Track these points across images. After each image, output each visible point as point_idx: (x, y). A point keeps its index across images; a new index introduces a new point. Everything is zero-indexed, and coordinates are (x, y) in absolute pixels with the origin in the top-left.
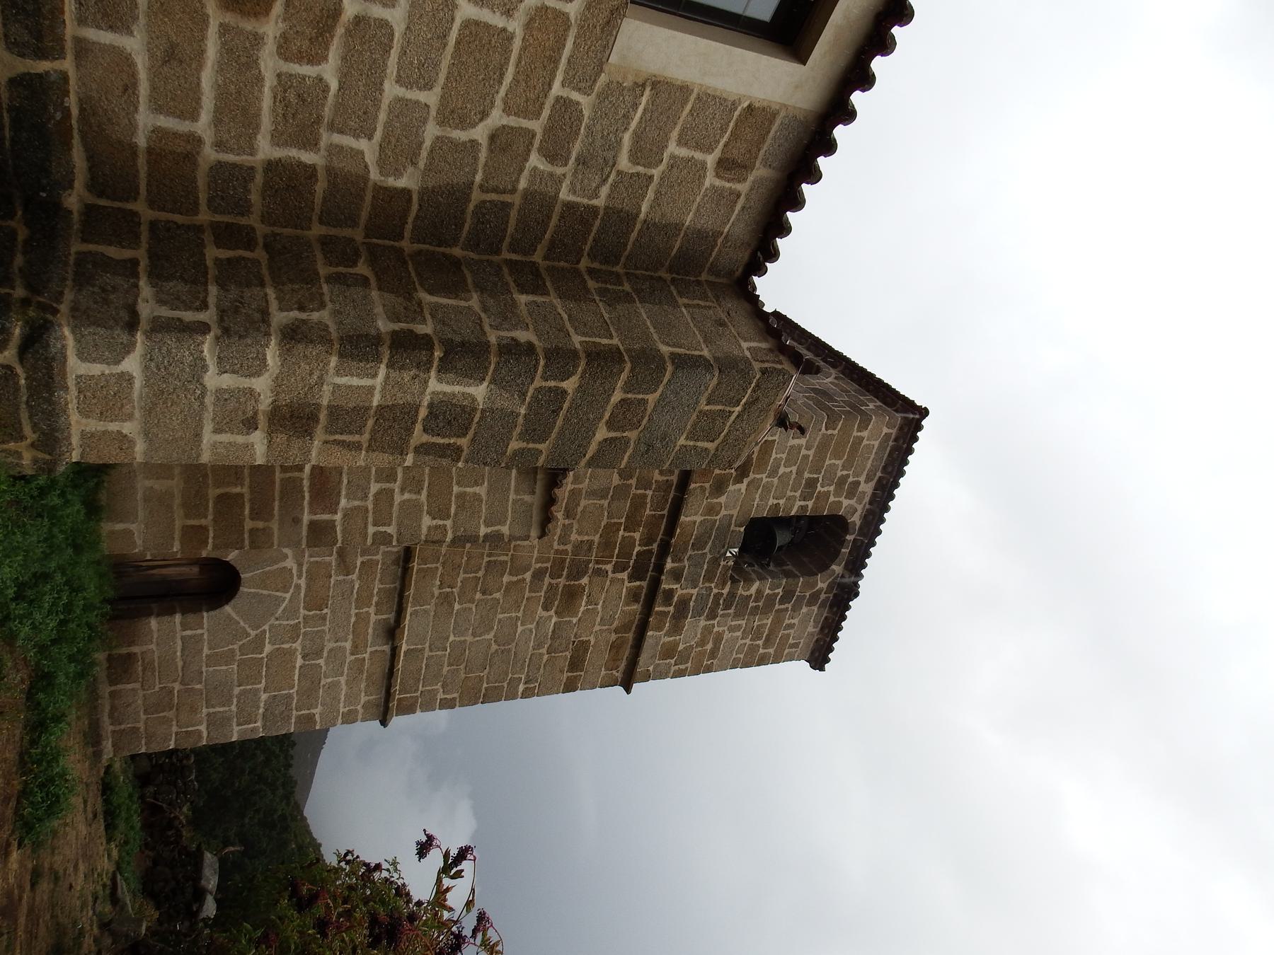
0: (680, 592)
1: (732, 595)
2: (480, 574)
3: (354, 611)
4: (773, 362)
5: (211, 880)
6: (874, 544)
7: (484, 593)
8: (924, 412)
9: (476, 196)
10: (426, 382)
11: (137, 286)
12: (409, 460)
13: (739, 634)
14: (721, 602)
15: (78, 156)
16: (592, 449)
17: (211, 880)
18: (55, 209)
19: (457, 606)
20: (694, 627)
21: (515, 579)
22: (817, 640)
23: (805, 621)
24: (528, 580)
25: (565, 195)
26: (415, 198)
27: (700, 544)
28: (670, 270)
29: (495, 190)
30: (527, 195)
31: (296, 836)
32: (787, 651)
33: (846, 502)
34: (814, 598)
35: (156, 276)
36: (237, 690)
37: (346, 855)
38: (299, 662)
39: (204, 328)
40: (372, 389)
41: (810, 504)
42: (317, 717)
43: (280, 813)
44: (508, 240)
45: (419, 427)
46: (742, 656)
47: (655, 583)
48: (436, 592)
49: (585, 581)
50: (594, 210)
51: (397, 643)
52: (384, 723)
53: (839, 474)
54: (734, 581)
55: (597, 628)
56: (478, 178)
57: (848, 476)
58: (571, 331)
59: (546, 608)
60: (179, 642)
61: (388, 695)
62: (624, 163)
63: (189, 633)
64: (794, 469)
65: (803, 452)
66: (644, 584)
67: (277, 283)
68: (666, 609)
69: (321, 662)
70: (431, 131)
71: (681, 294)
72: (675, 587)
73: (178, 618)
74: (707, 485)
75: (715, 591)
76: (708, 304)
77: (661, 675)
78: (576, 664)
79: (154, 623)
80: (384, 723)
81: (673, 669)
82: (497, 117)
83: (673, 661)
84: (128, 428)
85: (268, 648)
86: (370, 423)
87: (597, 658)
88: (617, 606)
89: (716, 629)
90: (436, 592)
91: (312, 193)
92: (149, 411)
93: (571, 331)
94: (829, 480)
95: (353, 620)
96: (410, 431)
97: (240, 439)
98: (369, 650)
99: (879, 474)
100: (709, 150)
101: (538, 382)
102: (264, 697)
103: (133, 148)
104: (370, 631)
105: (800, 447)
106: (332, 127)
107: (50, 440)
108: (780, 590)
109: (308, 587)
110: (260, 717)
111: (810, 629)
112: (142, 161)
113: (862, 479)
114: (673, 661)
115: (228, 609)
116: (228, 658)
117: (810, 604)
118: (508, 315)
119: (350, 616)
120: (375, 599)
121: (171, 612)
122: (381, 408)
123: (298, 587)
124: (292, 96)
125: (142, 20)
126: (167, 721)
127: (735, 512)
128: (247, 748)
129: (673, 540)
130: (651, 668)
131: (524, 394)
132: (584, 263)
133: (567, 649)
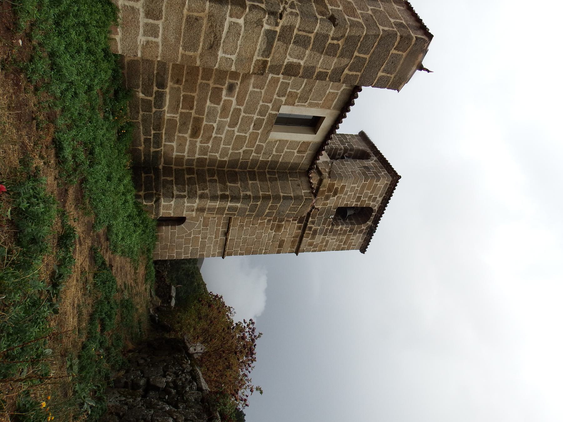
0: (314, 227)
1: (332, 229)
2: (252, 220)
3: (215, 228)
4: (309, 196)
5: (174, 294)
6: (381, 217)
7: (253, 225)
8: (400, 177)
9: (241, 161)
10: (227, 204)
11: (173, 187)
12: (224, 216)
13: (335, 241)
14: (328, 231)
15: (162, 160)
16: (266, 213)
17: (174, 294)
18: (158, 169)
19: (245, 228)
20: (318, 239)
21: (262, 221)
22: (362, 244)
23: (358, 239)
24: (266, 222)
25: (261, 159)
26: (227, 162)
27: (321, 214)
28: (289, 170)
29: (245, 159)
30: (252, 160)
31: (197, 280)
32: (351, 247)
33: (372, 203)
34: (361, 232)
35: (177, 184)
36: (184, 246)
37: (210, 293)
38: (200, 240)
39: (185, 196)
40: (216, 205)
41: (359, 203)
42: (205, 254)
43: (191, 272)
44: (248, 167)
45: (226, 211)
46: (336, 247)
47: (306, 225)
48: (239, 224)
49: (283, 223)
50: (268, 161)
51: (227, 237)
52: (223, 258)
53: (369, 195)
54: (333, 225)
55: (287, 236)
56: (241, 158)
57: (373, 195)
58: (260, 191)
59: (271, 230)
60: (170, 233)
61: (224, 251)
62: (274, 153)
63: (172, 231)
64: (353, 193)
65: (356, 188)
66: (302, 225)
67: (199, 184)
68: (310, 232)
69: (206, 240)
70: (230, 151)
71: (290, 177)
72: (312, 226)
73: (170, 227)
74: (323, 197)
75: (326, 228)
76: (297, 179)
77: (308, 251)
78: (280, 246)
79: (164, 228)
80: (223, 258)
81: (312, 249)
82: (244, 148)
83: (312, 247)
84: (170, 212)
85: (192, 236)
86: (216, 210)
87: (287, 245)
88: (294, 230)
89: (327, 239)
90: (239, 224)
91: (206, 162)
92: (174, 209)
93: (260, 191)
94: (366, 196)
95: (215, 230)
96: (224, 211)
97: (191, 213)
98: (219, 238)
99: (384, 195)
100: (295, 149)
101: (251, 203)
102: (191, 248)
103: (172, 158)
104: (220, 233)
105: (355, 187)
106: (210, 152)
107: (157, 214)
108: (349, 228)
109: (203, 221)
110: (190, 253)
111: (360, 240)
112: (174, 160)
113: (378, 196)
114: (312, 247)
115: (182, 225)
116: (182, 237)
117: (359, 233)
118: (246, 188)
119: (214, 229)
120: (222, 225)
121: (168, 225)
122: (218, 208)
123: (201, 221)
124: (202, 149)
125: (176, 141)
126: (166, 252)
127: (333, 205)
128: (188, 261)
129: (312, 213)
130: (305, 249)
131: (249, 205)
132: (267, 170)
133: (278, 241)
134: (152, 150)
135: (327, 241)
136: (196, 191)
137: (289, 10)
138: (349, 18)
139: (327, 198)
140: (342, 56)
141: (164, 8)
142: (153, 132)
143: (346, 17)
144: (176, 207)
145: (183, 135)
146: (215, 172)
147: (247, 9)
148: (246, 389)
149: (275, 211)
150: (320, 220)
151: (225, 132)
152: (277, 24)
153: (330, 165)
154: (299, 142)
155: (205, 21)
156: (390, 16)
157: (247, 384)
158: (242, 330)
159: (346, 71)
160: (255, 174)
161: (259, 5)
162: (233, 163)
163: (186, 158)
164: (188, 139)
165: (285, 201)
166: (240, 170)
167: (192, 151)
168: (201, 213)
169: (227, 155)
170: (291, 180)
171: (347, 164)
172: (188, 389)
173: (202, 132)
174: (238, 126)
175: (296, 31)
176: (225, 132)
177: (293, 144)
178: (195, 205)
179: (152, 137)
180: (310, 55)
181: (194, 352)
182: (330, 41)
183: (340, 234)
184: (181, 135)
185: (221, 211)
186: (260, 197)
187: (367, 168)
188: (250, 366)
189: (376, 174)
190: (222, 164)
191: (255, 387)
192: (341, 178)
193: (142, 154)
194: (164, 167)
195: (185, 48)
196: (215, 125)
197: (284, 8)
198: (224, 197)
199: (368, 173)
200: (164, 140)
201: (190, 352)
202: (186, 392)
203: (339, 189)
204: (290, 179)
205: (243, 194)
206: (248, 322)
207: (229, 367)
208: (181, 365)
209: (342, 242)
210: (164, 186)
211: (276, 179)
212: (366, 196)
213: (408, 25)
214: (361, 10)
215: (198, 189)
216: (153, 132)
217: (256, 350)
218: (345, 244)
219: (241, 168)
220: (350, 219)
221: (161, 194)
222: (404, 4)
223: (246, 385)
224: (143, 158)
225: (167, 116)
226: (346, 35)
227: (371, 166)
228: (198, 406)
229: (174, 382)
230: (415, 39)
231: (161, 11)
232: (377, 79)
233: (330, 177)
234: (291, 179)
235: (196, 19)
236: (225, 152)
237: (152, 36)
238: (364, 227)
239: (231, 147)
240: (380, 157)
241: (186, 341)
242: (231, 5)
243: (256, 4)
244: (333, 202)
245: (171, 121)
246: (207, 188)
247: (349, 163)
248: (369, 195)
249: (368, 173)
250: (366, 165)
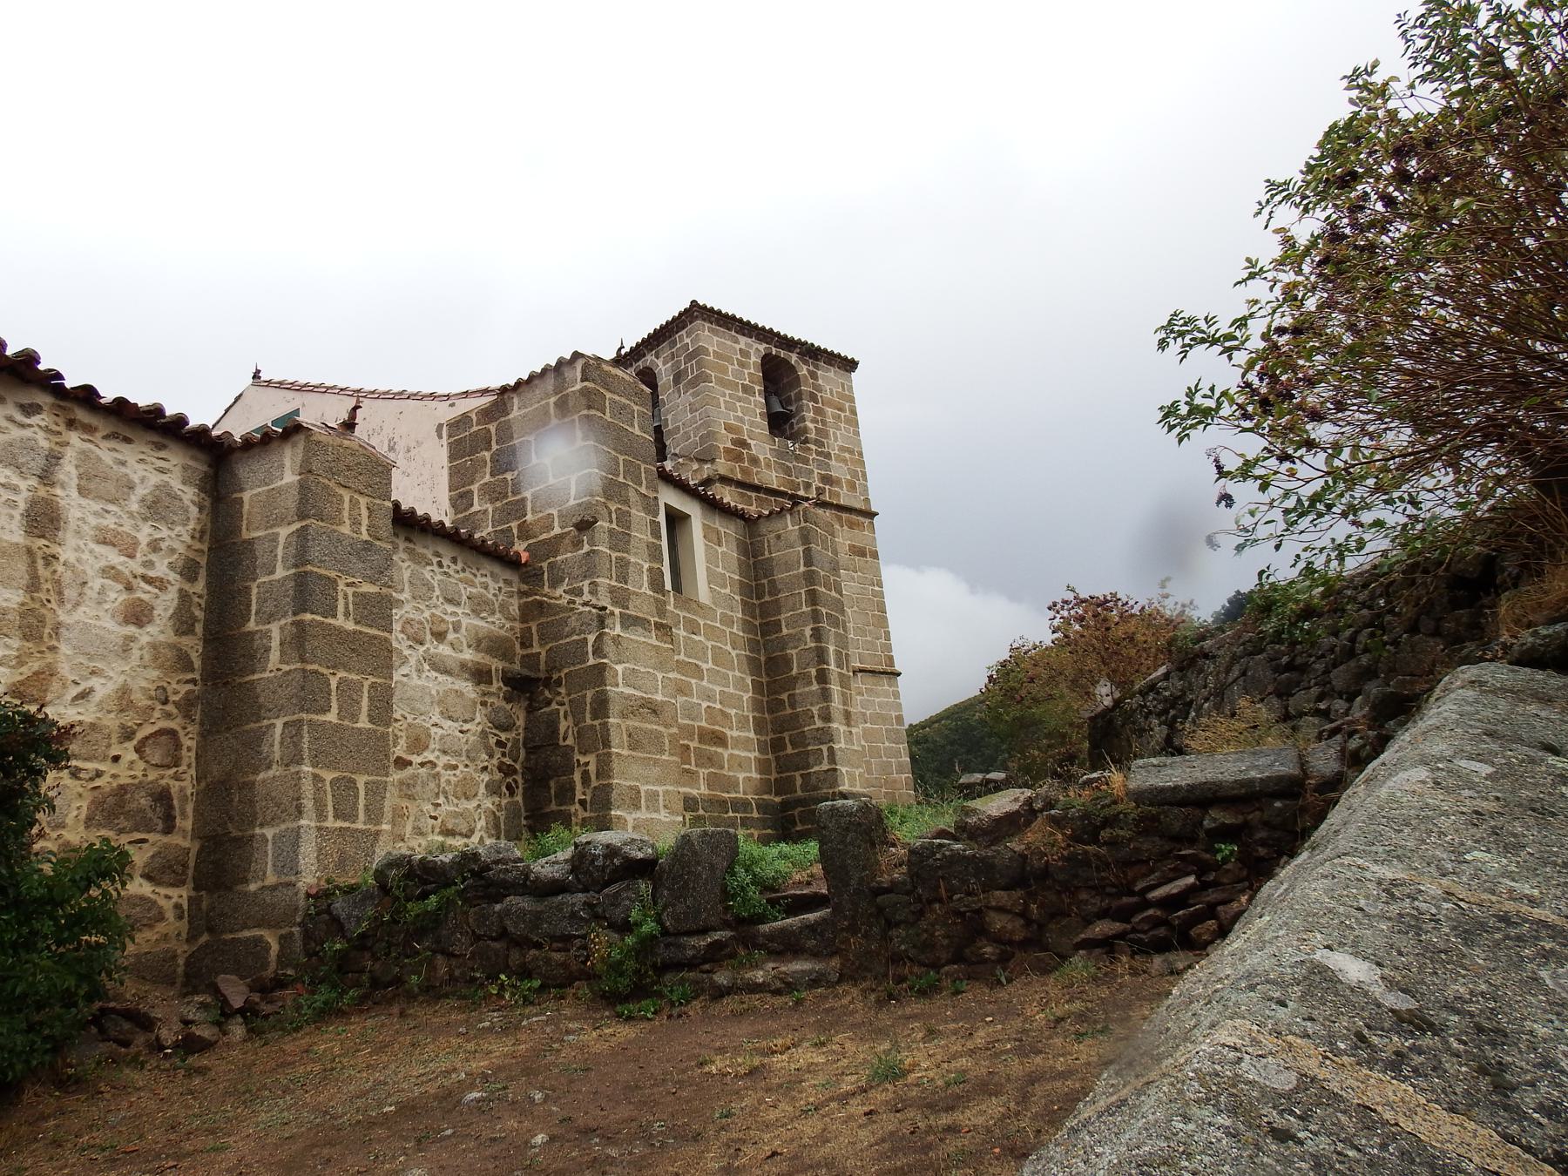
1: (817, 442)
8: (694, 304)
15: (765, 797)
16: (838, 596)
18: (783, 803)
20: (838, 470)
23: (828, 377)
33: (753, 359)
34: (813, 375)
35: (808, 766)
38: (868, 725)
41: (757, 388)
52: (899, 674)
54: (806, 441)
64: (738, 404)
65: (727, 399)
67: (802, 726)
70: (737, 674)
71: (763, 554)
78: (861, 552)
80: (899, 674)
82: (729, 648)
94: (740, 375)
105: (725, 402)
113: (738, 347)
117: (816, 379)
118: (798, 638)
126: (900, 795)
127: (768, 447)
134: (755, 815)
135: (842, 449)
136: (818, 729)
137: (586, 597)
139: (754, 461)
140: (626, 502)
141: (628, 784)
142: (731, 814)
144: (849, 763)
150: (800, 472)
152: (612, 614)
155: (629, 723)
157: (1156, 604)
160: (767, 624)
162: (754, 666)
163: (757, 754)
164: (730, 751)
165: (815, 562)
167: (743, 743)
169: (743, 679)
170: (770, 553)
171: (675, 420)
172: (1167, 694)
173: (717, 728)
174: (700, 663)
175: (614, 583)
177: (711, 558)
178: (843, 728)
179: (738, 815)
180: (636, 554)
181: (1110, 698)
183: (824, 423)
187: (678, 378)
189: (690, 357)
190: (757, 687)
191: (1160, 591)
192: (711, 435)
195: (662, 752)
196: (705, 705)
197: (585, 604)
198: (822, 677)
199: (692, 373)
204: (767, 554)
206: (1052, 613)
207: (1131, 638)
208: (1135, 711)
209: (839, 416)
210: (816, 788)
211: (772, 583)
212: (740, 375)
216: (731, 814)
220: (789, 401)
224: (769, 831)
228: (1189, 674)
229: (1159, 715)
230: (586, 383)
231: (631, 788)
233: (713, 461)
235: (630, 736)
236: (740, 683)
238: (803, 371)
239: (730, 673)
243: (590, 649)
244: (762, 446)
245: (712, 781)
247: (669, 417)
249: (692, 373)
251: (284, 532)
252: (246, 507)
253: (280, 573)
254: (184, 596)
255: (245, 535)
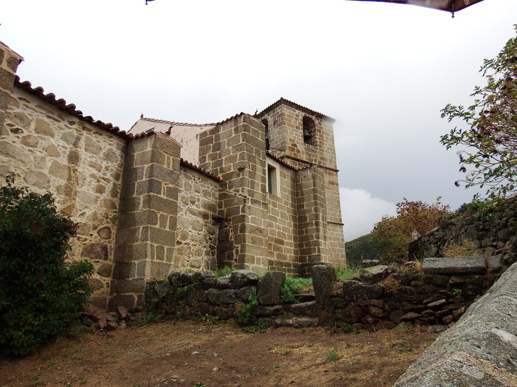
1: (320, 146)
9: (292, 214)
15: (296, 262)
20: (326, 155)
25: (291, 202)
33: (300, 117)
34: (320, 124)
35: (311, 253)
36: (337, 253)
38: (332, 241)
41: (301, 127)
52: (343, 225)
54: (316, 145)
62: (287, 194)
64: (294, 132)
65: (291, 130)
70: (289, 221)
74: (298, 154)
75: (319, 150)
77: (335, 162)
78: (333, 183)
82: (286, 212)
87: (332, 178)
89: (326, 149)
92: (326, 254)
96: (324, 224)
99: (294, 109)
102: (338, 248)
105: (290, 131)
112: (296, 256)
113: (295, 113)
118: (310, 211)
126: (342, 265)
127: (303, 147)
134: (292, 268)
135: (328, 148)
136: (315, 241)
137: (240, 193)
138: (238, 160)
139: (298, 151)
140: (255, 162)
141: (251, 255)
143: (237, 162)
145: (283, 249)
146: (300, 230)
147: (245, 214)
148: (438, 207)
149: (322, 191)
151: (280, 225)
152: (248, 199)
153: (274, 150)
154: (281, 178)
155: (252, 235)
156: (230, 136)
157: (435, 206)
158: (403, 210)
159: (261, 159)
160: (300, 205)
161: (241, 208)
162: (294, 219)
163: (294, 248)
166: (297, 214)
168: (327, 238)
169: (291, 223)
173: (281, 238)
174: (276, 217)
176: (280, 225)
177: (282, 182)
178: (323, 241)
179: (287, 268)
180: (257, 179)
181: (417, 237)
182: (251, 170)
183: (322, 140)
184: (283, 251)
185: (324, 226)
186: (315, 202)
187: (275, 123)
188: (425, 205)
189: (279, 116)
190: (295, 226)
192: (284, 142)
193: (295, 274)
194: (300, 262)
195: (262, 245)
196: (277, 231)
198: (317, 224)
199: (280, 121)
200: (287, 261)
201: (417, 239)
202: (439, 237)
203: (292, 143)
204: (301, 182)
205: (314, 212)
206: (398, 207)
207: (426, 217)
209: (328, 138)
210: (313, 261)
213: (235, 126)
214: (230, 153)
215: (313, 240)
216: (284, 267)
217: (415, 201)
218: (329, 136)
219: (296, 214)
220: (311, 132)
221: (318, 262)
222: (219, 126)
223: (436, 206)
224: (297, 274)
225: (276, 259)
226: (248, 161)
227: (273, 119)
228: (446, 230)
229: (434, 244)
230: (244, 123)
231: (251, 256)
232: (262, 140)
233: (285, 150)
234: (301, 182)
236: (289, 224)
237: (260, 261)
238: (317, 122)
239: (286, 221)
240: (265, 112)
241: (410, 242)
242: (245, 222)
243: (241, 210)
244: (301, 146)
245: (279, 256)
246: (312, 234)
247: (271, 136)
248: (294, 120)
250: (273, 123)
251: (146, 166)
252: (135, 157)
253: (144, 179)
254: (115, 185)
255: (135, 167)
